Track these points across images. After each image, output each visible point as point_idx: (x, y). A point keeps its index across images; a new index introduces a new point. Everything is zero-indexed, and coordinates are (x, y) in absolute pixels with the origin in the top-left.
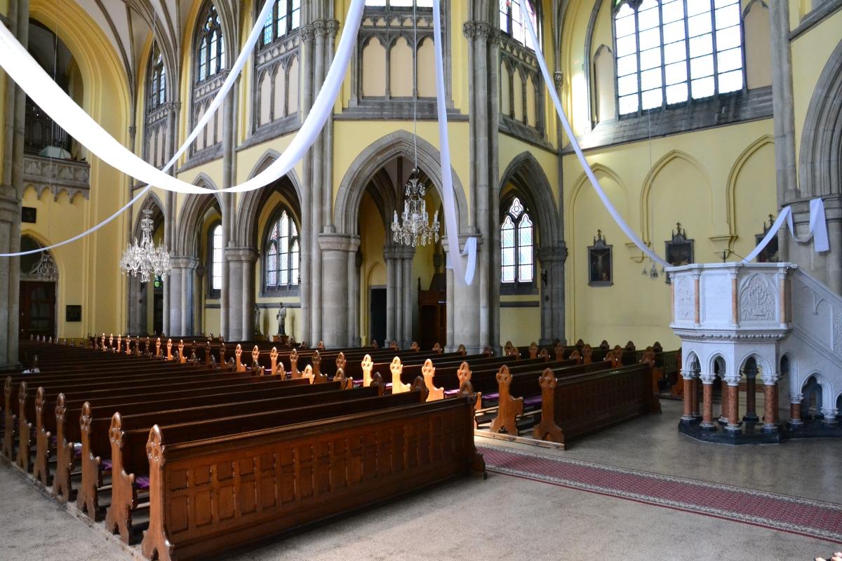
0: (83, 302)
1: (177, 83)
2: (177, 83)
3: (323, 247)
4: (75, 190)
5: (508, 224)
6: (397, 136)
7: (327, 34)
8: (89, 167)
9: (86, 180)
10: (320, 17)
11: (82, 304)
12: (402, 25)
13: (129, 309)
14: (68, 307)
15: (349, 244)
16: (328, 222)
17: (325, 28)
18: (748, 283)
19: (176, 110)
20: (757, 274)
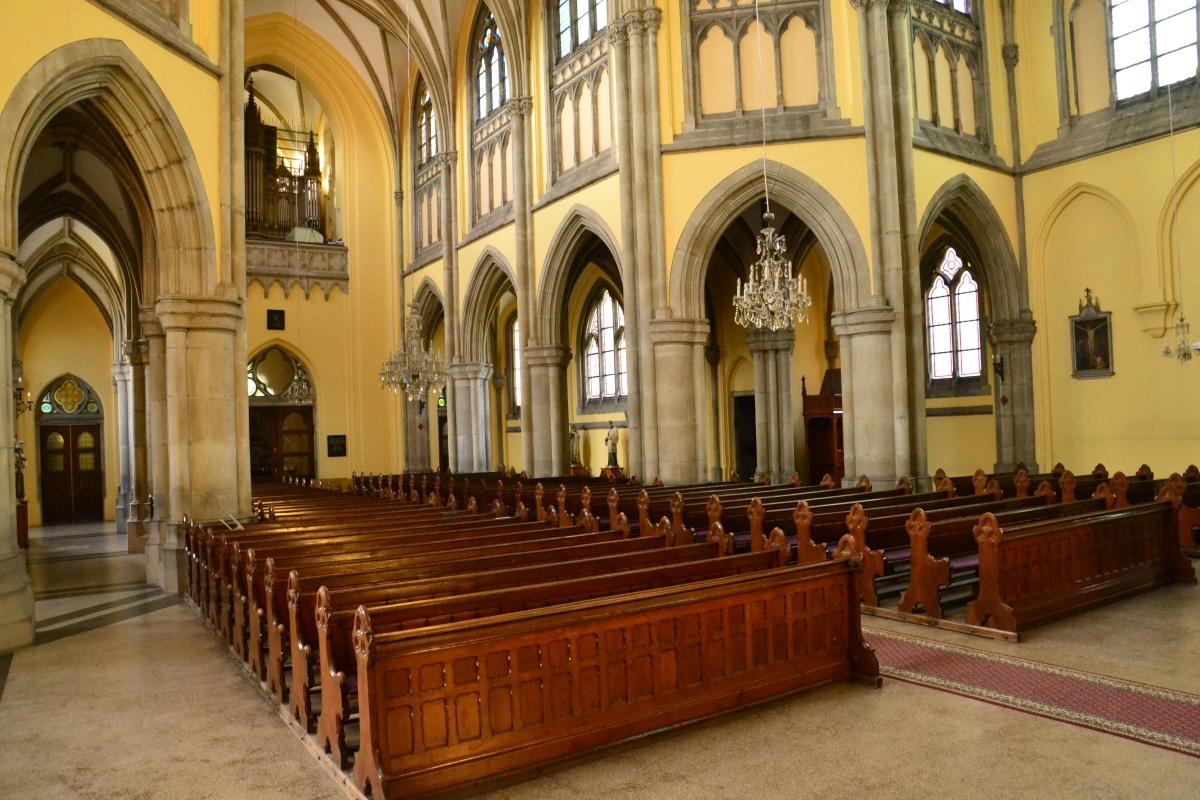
1: (451, 130)
2: (451, 130)
5: (939, 288)
7: (645, 30)
8: (346, 250)
9: (344, 268)
10: (633, 6)
14: (329, 437)
17: (642, 22)
19: (450, 162)
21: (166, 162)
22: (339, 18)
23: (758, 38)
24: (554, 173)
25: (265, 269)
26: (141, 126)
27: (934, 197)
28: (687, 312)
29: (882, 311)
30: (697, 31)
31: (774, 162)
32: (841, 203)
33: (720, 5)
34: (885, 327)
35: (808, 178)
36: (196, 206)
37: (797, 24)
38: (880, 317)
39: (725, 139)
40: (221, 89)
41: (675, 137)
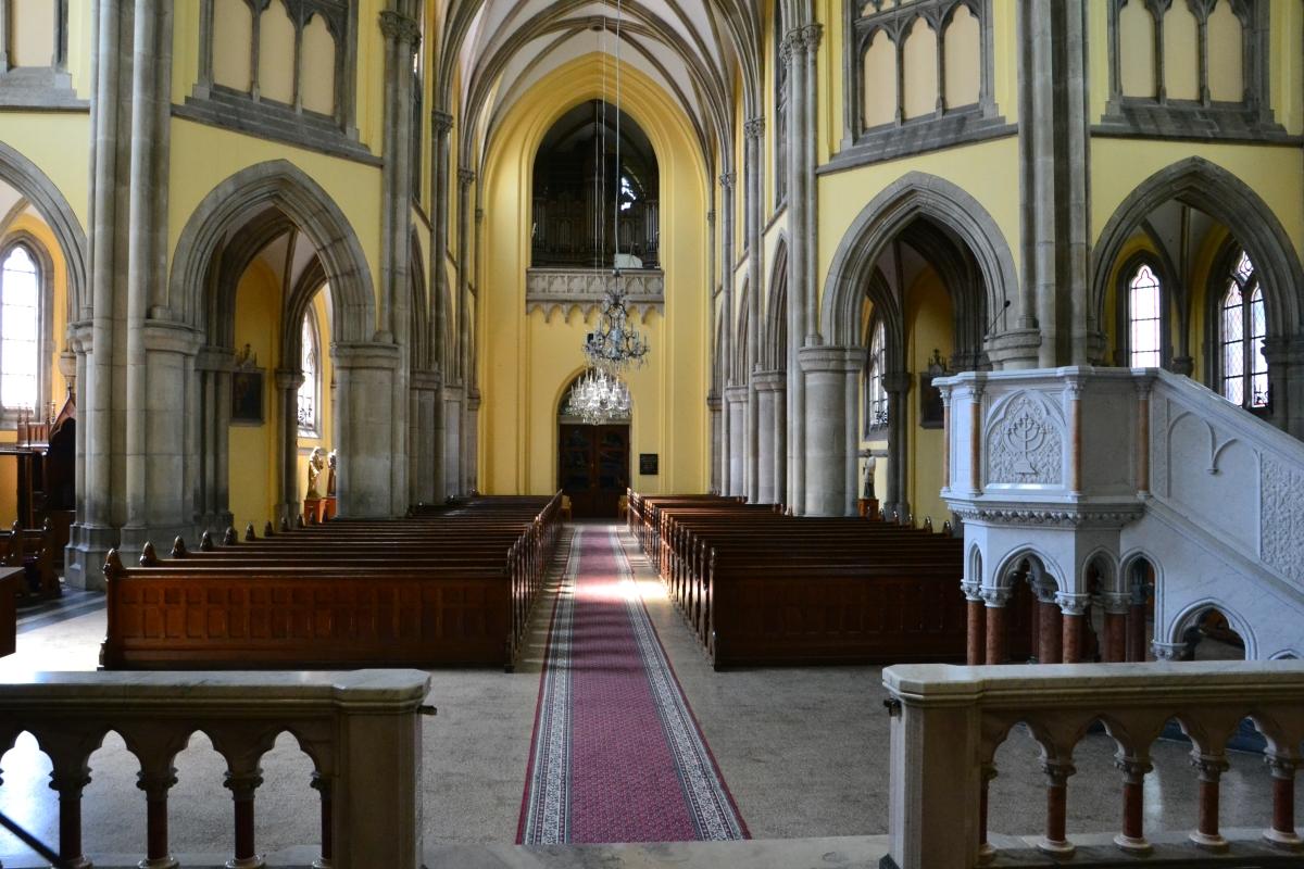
0: (659, 450)
1: (730, 151)
2: (730, 151)
3: (805, 367)
4: (647, 306)
5: (1235, 296)
6: (906, 182)
7: (805, 49)
8: (663, 274)
9: (660, 292)
11: (659, 453)
12: (878, 10)
13: (713, 459)
14: (642, 456)
15: (843, 361)
16: (810, 331)
17: (801, 41)
18: (1003, 412)
19: (730, 184)
20: (1023, 393)
21: (330, 241)
22: (643, 48)
23: (922, 37)
24: (778, 194)
25: (585, 296)
26: (307, 218)
27: (1135, 192)
28: (837, 338)
29: (1026, 334)
30: (860, 41)
31: (924, 174)
32: (991, 213)
33: (884, 7)
34: (1031, 352)
35: (957, 188)
36: (356, 272)
37: (963, 12)
38: (1021, 340)
39: (902, 149)
40: (383, 175)
41: (832, 156)
